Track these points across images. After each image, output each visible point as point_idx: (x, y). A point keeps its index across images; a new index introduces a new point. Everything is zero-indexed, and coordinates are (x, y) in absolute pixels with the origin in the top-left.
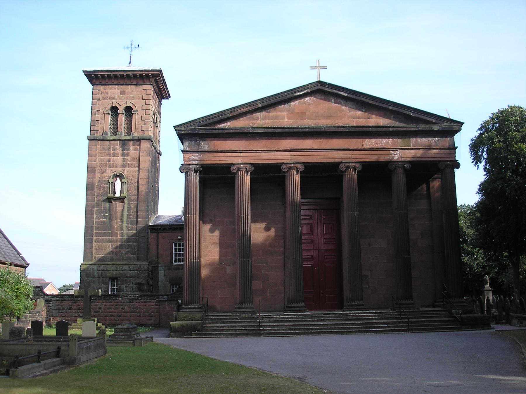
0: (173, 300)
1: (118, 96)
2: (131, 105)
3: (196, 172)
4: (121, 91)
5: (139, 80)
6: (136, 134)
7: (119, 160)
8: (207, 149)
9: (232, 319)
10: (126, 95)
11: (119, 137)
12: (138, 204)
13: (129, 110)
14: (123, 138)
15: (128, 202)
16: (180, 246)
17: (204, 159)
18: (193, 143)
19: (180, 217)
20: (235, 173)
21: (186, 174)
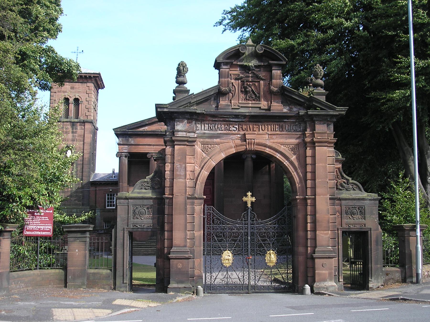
0: (108, 233)
1: (69, 91)
2: (78, 97)
3: (126, 157)
4: (71, 87)
5: (84, 80)
6: (82, 118)
7: (70, 136)
8: (133, 143)
9: (146, 246)
10: (75, 90)
11: (70, 120)
12: (83, 167)
13: (77, 101)
14: (72, 121)
15: (76, 166)
16: (111, 196)
17: (132, 149)
18: (124, 139)
19: (111, 175)
20: (150, 158)
21: (120, 158)
